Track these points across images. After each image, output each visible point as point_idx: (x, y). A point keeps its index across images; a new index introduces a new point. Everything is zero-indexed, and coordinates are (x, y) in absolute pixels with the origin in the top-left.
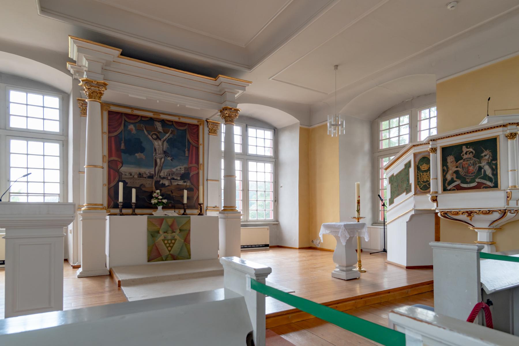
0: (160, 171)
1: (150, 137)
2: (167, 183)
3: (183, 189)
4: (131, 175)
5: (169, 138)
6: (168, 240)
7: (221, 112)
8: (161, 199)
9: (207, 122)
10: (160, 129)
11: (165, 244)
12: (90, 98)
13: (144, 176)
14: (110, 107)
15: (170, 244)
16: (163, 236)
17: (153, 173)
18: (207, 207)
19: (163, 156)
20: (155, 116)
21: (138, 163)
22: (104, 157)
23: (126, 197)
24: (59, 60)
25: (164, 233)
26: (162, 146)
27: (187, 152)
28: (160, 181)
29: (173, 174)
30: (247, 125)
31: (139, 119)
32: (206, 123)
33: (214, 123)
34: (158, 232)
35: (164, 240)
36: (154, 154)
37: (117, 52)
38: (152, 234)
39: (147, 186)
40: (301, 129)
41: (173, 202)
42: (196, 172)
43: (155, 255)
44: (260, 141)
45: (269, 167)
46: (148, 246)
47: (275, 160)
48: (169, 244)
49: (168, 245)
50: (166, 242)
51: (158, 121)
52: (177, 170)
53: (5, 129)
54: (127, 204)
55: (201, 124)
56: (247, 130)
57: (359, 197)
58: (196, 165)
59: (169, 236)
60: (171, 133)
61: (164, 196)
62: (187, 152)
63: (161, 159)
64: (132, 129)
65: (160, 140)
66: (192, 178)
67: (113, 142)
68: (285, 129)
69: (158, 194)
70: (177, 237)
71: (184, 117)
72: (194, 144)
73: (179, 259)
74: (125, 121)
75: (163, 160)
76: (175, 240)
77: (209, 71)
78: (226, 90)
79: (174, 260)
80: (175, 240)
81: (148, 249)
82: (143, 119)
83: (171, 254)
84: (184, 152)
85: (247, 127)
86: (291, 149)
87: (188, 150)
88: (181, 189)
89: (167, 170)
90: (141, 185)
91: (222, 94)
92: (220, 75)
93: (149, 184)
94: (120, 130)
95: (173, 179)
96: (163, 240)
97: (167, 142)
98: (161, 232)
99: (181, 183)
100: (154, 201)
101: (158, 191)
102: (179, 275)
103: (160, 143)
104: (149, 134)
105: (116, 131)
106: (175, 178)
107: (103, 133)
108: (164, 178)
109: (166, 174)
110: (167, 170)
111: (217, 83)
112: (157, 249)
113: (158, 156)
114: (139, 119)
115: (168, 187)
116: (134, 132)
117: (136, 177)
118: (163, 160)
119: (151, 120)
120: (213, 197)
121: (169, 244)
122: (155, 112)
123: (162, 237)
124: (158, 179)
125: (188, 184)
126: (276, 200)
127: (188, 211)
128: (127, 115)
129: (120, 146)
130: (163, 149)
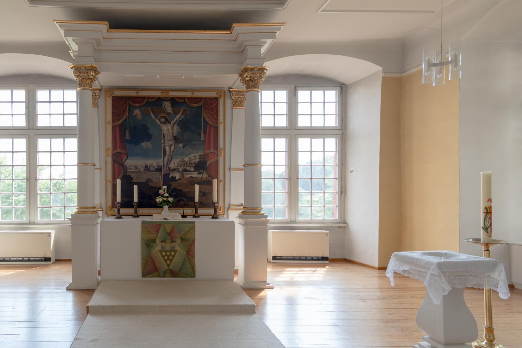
0: (169, 162)
1: (157, 121)
2: (177, 176)
3: (194, 184)
4: (137, 168)
5: (180, 119)
6: (166, 252)
7: (241, 75)
8: (167, 197)
9: (230, 91)
10: (169, 109)
11: (163, 256)
12: (80, 87)
13: (152, 169)
14: (113, 92)
15: (169, 256)
16: (160, 245)
17: (161, 164)
18: (229, 205)
19: (172, 142)
20: (164, 95)
21: (145, 154)
22: (107, 150)
23: (135, 194)
24: (59, 50)
25: (162, 242)
26: (171, 131)
27: (202, 135)
28: (169, 174)
29: (185, 164)
30: (295, 87)
31: (145, 101)
32: (228, 94)
33: (239, 92)
34: (154, 241)
35: (161, 252)
36: (162, 142)
37: (103, 26)
38: (148, 244)
39: (154, 180)
40: (384, 79)
41: (181, 199)
42: (215, 159)
43: (150, 268)
44: (318, 107)
45: (331, 143)
46: (143, 258)
47: (342, 133)
48: (168, 256)
49: (166, 258)
50: (164, 253)
51: (167, 101)
52: (190, 158)
53: (33, 129)
54: (127, 203)
55: (220, 96)
56: (295, 94)
57: (490, 200)
58: (214, 151)
59: (168, 247)
60: (183, 114)
61: (172, 192)
62: (202, 135)
63: (170, 147)
64: (137, 114)
65: (170, 123)
66: (208, 169)
67: (118, 138)
68: (356, 84)
69: (164, 190)
70: (177, 248)
71: (198, 90)
72: (212, 123)
73: (180, 277)
74: (130, 105)
75: (173, 147)
76: (176, 252)
77: (220, 23)
78: (246, 43)
79: (174, 277)
80: (176, 252)
81: (142, 261)
82: (150, 100)
83: (169, 269)
84: (199, 134)
85: (295, 89)
86: (368, 115)
87: (205, 133)
88: (192, 182)
89: (178, 160)
90: (147, 180)
91: (241, 51)
92: (234, 25)
93: (157, 179)
94: (124, 118)
95: (186, 170)
96: (160, 251)
97: (178, 125)
98: (158, 241)
99: (195, 175)
100: (159, 200)
101: (165, 187)
102: (160, 307)
103: (169, 127)
104: (156, 118)
105: (120, 119)
106: (188, 169)
107: (106, 123)
108: (174, 170)
109: (176, 165)
110: (178, 160)
111: (233, 36)
112: (153, 263)
113: (167, 143)
114: (145, 101)
115: (180, 181)
116: (140, 117)
117: (142, 170)
118: (173, 147)
119: (159, 100)
120: (232, 192)
121: (168, 256)
122: (192, 90)
123: (159, 248)
124: (167, 172)
125: (205, 175)
126: (343, 191)
127: (200, 211)
128: (132, 98)
129: (125, 137)
130: (173, 133)
